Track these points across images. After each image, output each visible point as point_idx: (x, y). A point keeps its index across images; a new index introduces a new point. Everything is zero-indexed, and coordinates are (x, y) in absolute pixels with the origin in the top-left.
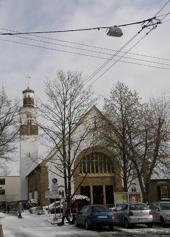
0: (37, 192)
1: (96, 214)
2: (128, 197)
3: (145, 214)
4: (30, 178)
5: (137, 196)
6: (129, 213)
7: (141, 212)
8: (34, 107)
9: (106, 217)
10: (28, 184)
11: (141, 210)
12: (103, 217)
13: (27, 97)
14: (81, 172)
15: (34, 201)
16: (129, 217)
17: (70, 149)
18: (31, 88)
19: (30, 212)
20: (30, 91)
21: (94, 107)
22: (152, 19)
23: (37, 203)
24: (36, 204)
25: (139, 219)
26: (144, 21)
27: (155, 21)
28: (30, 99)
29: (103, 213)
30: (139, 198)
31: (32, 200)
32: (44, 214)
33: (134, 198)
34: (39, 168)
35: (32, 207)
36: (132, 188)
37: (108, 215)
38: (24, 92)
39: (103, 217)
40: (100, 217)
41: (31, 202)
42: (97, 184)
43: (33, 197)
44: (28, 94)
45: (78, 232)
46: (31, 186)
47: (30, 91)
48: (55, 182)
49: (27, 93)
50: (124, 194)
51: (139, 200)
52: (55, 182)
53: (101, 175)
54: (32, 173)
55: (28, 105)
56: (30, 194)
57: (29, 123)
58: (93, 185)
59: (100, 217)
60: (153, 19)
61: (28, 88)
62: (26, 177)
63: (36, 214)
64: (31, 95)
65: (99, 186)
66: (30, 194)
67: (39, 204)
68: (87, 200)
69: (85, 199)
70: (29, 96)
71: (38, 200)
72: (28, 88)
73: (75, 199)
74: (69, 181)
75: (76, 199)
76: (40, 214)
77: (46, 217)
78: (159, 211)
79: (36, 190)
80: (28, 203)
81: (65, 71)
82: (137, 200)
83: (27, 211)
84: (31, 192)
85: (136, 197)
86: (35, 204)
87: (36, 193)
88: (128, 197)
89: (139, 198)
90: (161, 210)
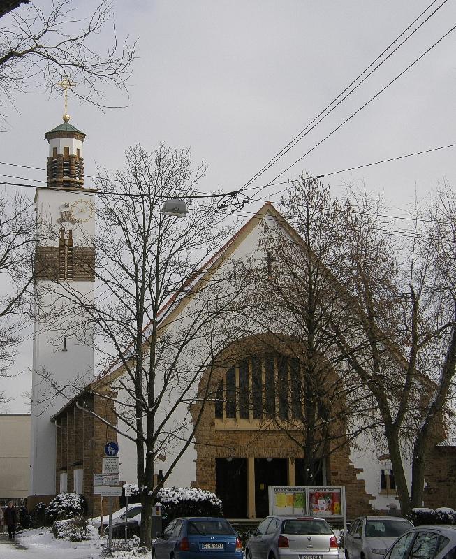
0: (66, 474)
1: (195, 539)
2: (308, 499)
3: (320, 545)
4: (65, 425)
5: (332, 498)
6: (279, 540)
7: (310, 539)
8: (85, 186)
9: (221, 547)
10: (59, 444)
11: (309, 534)
12: (214, 547)
13: (61, 152)
14: (219, 415)
15: (69, 499)
16: (278, 551)
17: (153, 365)
18: (75, 123)
19: (53, 535)
20: (73, 133)
21: (268, 207)
22: (236, 192)
23: (76, 505)
24: (75, 510)
25: (302, 555)
26: (224, 195)
27: (241, 198)
28: (70, 158)
29: (212, 538)
30: (336, 504)
31: (62, 496)
32: (89, 539)
33: (322, 503)
34: (86, 396)
35: (58, 517)
36: (383, 471)
37: (225, 543)
38: (50, 136)
39: (214, 547)
40: (207, 547)
41: (60, 504)
42: (270, 455)
43: (70, 489)
44: (63, 142)
45: (46, 546)
46: (64, 452)
47: (73, 133)
48: (111, 453)
49: (62, 139)
50: (296, 492)
51: (338, 508)
52: (111, 453)
53: (285, 425)
54: (68, 411)
55: (64, 181)
56: (64, 477)
57: (66, 242)
58: (256, 456)
59: (207, 547)
60: (238, 192)
61: (66, 120)
62: (52, 421)
63: (68, 538)
64: (75, 145)
65: (274, 460)
66: (64, 477)
67: (87, 508)
68: (211, 503)
69: (207, 502)
70: (67, 149)
71: (83, 497)
72: (66, 120)
73: (178, 499)
74: (148, 451)
75: (181, 499)
76: (78, 540)
77: (93, 547)
78: (360, 538)
79: (79, 464)
80: (52, 507)
81: (150, 149)
82: (331, 508)
83: (46, 532)
84: (64, 469)
85: (329, 502)
86: (70, 509)
87: (78, 474)
88: (308, 499)
89: (336, 504)
90: (366, 536)
